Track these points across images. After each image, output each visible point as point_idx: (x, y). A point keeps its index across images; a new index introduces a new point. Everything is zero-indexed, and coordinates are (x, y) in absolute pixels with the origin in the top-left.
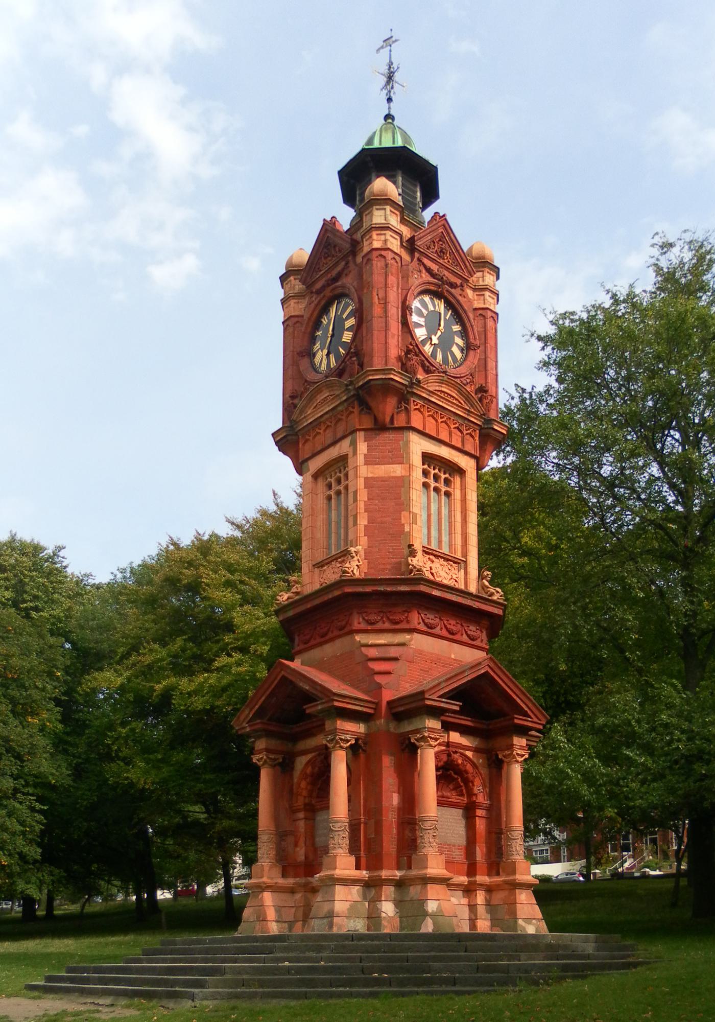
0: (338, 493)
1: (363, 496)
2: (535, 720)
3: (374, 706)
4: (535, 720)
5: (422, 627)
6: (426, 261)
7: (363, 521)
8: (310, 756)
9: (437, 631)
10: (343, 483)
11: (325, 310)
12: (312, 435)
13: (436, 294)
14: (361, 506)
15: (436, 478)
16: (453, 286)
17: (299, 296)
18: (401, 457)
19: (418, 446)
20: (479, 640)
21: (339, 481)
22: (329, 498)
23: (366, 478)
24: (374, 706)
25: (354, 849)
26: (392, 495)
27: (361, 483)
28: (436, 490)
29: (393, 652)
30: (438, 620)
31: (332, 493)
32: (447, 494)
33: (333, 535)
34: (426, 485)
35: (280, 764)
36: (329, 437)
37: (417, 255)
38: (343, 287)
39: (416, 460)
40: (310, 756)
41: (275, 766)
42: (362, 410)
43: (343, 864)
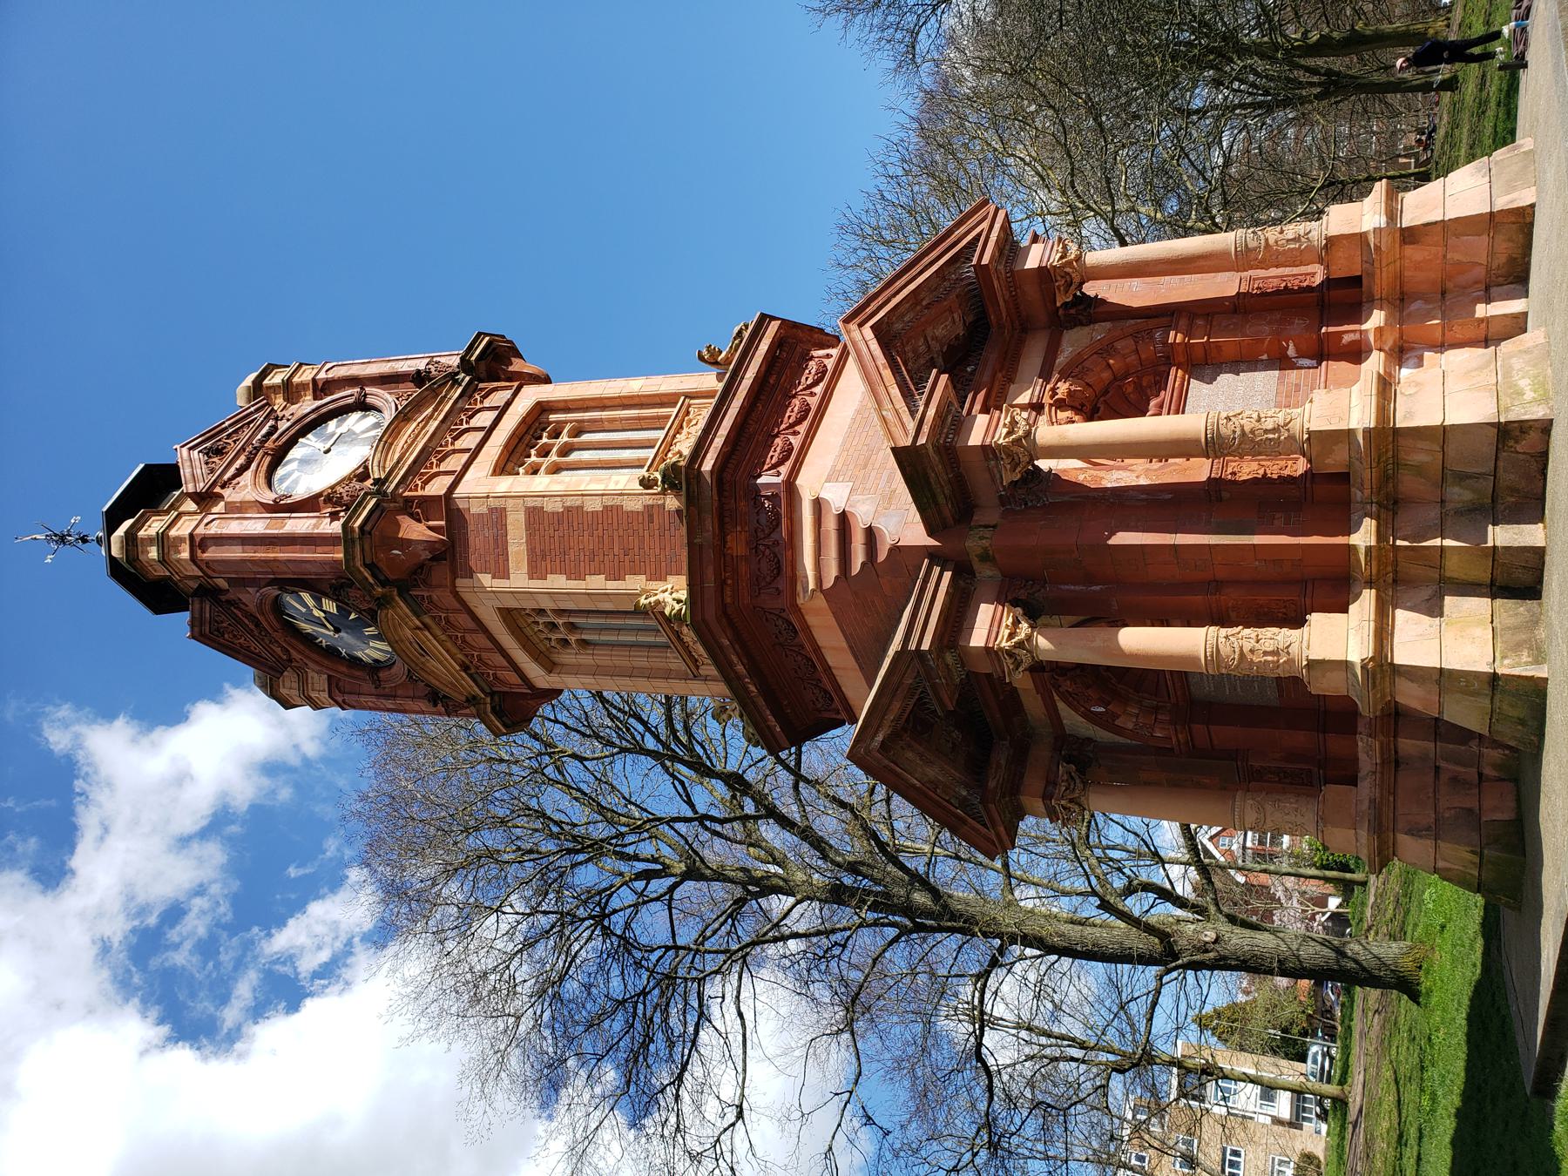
0: (572, 627)
1: (558, 582)
2: (985, 225)
3: (937, 570)
4: (985, 225)
5: (784, 470)
6: (226, 477)
7: (597, 583)
8: (1061, 705)
9: (796, 442)
10: (552, 618)
11: (309, 640)
12: (483, 669)
13: (278, 457)
14: (613, 586)
15: (545, 453)
16: (274, 428)
17: (303, 682)
18: (498, 516)
19: (480, 484)
20: (826, 361)
21: (553, 626)
22: (584, 643)
23: (531, 578)
24: (937, 570)
25: (1013, 693)
26: (562, 535)
27: (536, 585)
28: (566, 451)
29: (830, 525)
30: (778, 441)
31: (572, 638)
32: (577, 432)
33: (641, 639)
34: (556, 469)
35: (1082, 771)
36: (480, 640)
37: (218, 490)
38: (260, 605)
39: (505, 484)
40: (1061, 705)
41: (1084, 783)
42: (424, 582)
43: (1337, 638)
